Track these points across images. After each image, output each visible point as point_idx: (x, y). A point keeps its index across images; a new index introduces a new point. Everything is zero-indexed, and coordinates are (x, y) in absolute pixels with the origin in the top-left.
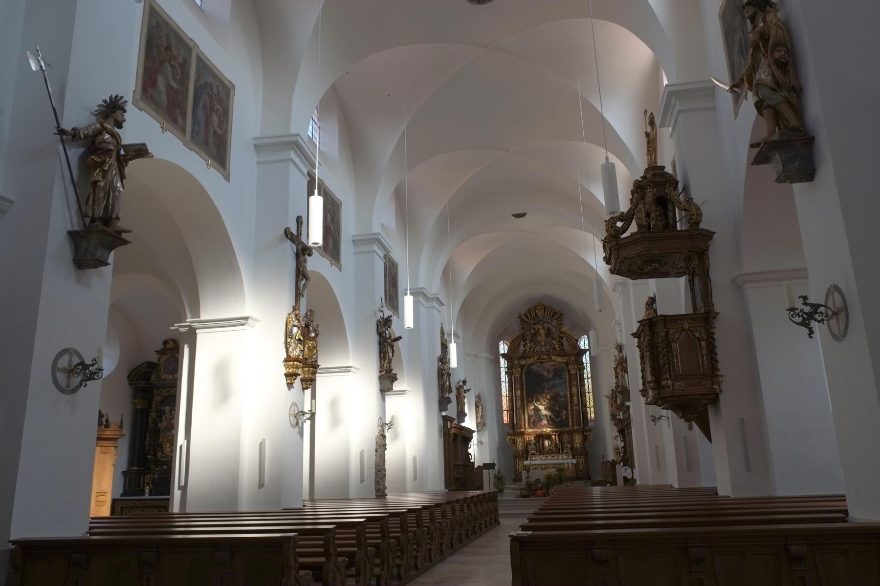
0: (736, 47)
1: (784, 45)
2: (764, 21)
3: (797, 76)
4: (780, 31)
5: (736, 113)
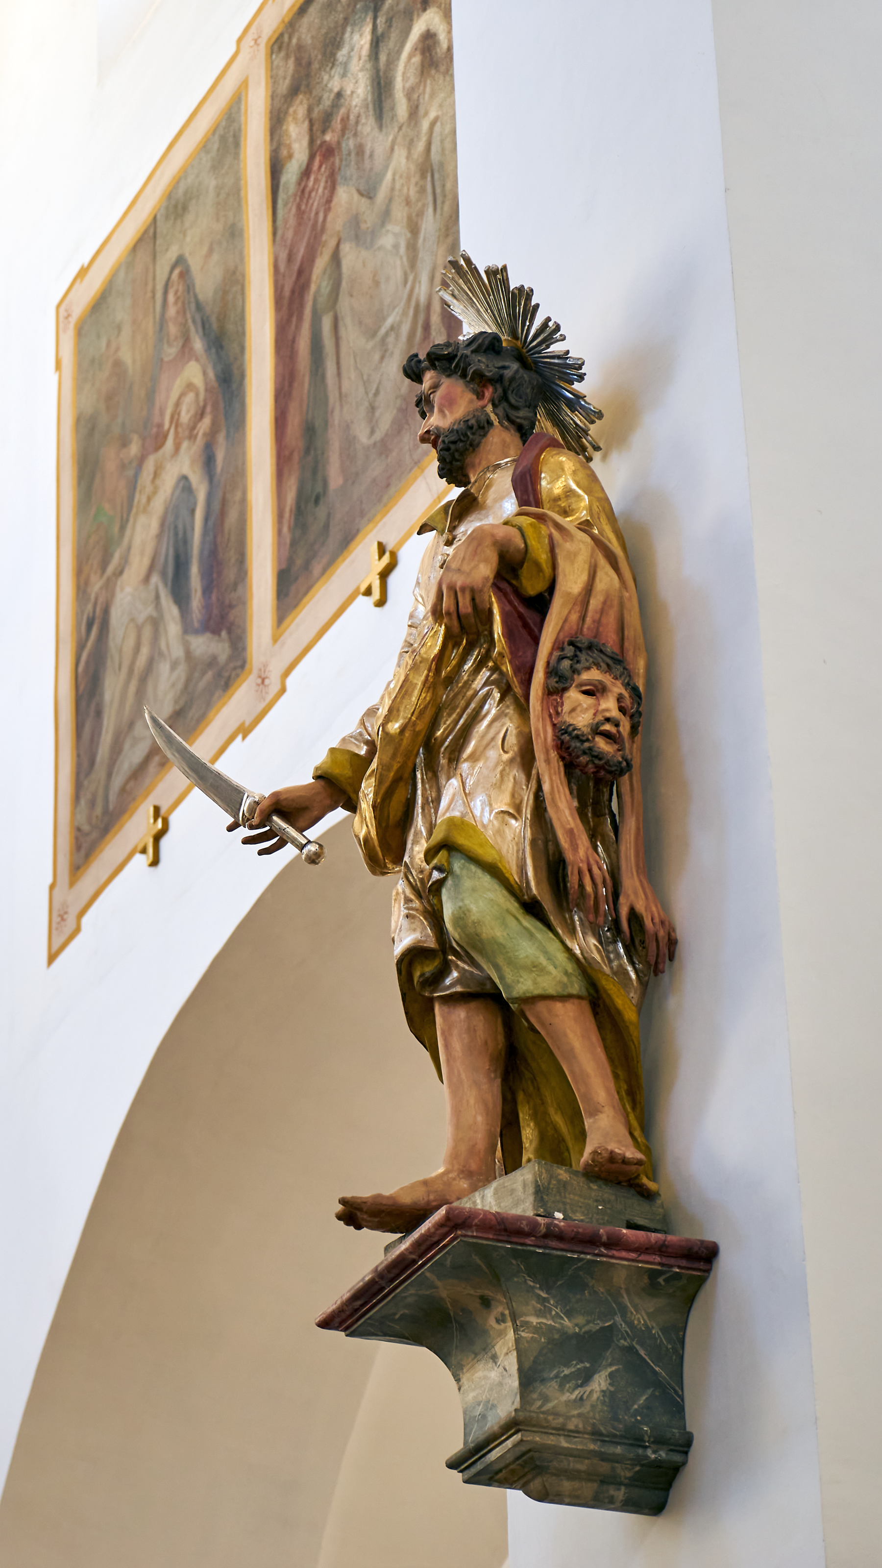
0: (144, 534)
1: (616, 663)
2: (526, 488)
3: (653, 862)
4: (607, 579)
5: (63, 929)
